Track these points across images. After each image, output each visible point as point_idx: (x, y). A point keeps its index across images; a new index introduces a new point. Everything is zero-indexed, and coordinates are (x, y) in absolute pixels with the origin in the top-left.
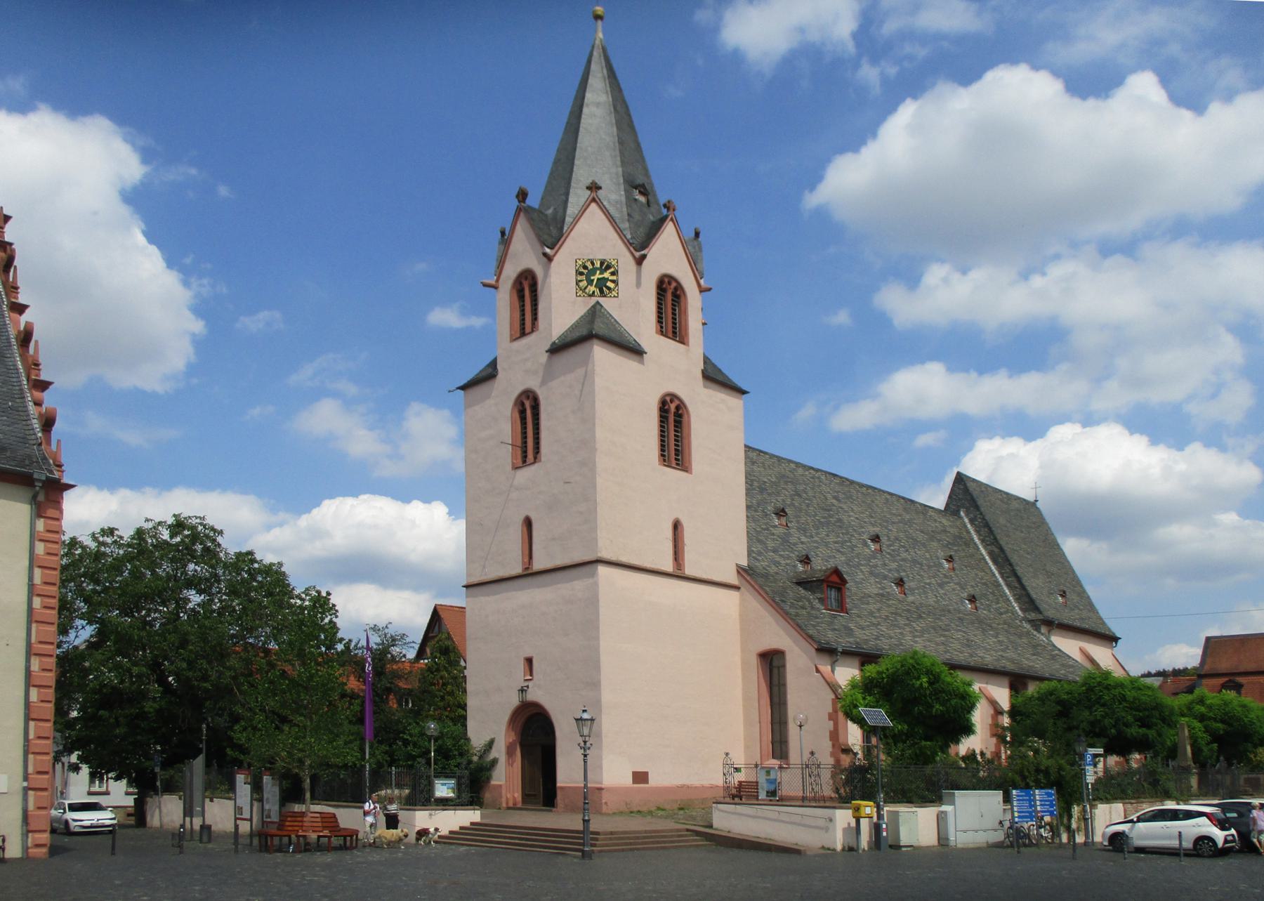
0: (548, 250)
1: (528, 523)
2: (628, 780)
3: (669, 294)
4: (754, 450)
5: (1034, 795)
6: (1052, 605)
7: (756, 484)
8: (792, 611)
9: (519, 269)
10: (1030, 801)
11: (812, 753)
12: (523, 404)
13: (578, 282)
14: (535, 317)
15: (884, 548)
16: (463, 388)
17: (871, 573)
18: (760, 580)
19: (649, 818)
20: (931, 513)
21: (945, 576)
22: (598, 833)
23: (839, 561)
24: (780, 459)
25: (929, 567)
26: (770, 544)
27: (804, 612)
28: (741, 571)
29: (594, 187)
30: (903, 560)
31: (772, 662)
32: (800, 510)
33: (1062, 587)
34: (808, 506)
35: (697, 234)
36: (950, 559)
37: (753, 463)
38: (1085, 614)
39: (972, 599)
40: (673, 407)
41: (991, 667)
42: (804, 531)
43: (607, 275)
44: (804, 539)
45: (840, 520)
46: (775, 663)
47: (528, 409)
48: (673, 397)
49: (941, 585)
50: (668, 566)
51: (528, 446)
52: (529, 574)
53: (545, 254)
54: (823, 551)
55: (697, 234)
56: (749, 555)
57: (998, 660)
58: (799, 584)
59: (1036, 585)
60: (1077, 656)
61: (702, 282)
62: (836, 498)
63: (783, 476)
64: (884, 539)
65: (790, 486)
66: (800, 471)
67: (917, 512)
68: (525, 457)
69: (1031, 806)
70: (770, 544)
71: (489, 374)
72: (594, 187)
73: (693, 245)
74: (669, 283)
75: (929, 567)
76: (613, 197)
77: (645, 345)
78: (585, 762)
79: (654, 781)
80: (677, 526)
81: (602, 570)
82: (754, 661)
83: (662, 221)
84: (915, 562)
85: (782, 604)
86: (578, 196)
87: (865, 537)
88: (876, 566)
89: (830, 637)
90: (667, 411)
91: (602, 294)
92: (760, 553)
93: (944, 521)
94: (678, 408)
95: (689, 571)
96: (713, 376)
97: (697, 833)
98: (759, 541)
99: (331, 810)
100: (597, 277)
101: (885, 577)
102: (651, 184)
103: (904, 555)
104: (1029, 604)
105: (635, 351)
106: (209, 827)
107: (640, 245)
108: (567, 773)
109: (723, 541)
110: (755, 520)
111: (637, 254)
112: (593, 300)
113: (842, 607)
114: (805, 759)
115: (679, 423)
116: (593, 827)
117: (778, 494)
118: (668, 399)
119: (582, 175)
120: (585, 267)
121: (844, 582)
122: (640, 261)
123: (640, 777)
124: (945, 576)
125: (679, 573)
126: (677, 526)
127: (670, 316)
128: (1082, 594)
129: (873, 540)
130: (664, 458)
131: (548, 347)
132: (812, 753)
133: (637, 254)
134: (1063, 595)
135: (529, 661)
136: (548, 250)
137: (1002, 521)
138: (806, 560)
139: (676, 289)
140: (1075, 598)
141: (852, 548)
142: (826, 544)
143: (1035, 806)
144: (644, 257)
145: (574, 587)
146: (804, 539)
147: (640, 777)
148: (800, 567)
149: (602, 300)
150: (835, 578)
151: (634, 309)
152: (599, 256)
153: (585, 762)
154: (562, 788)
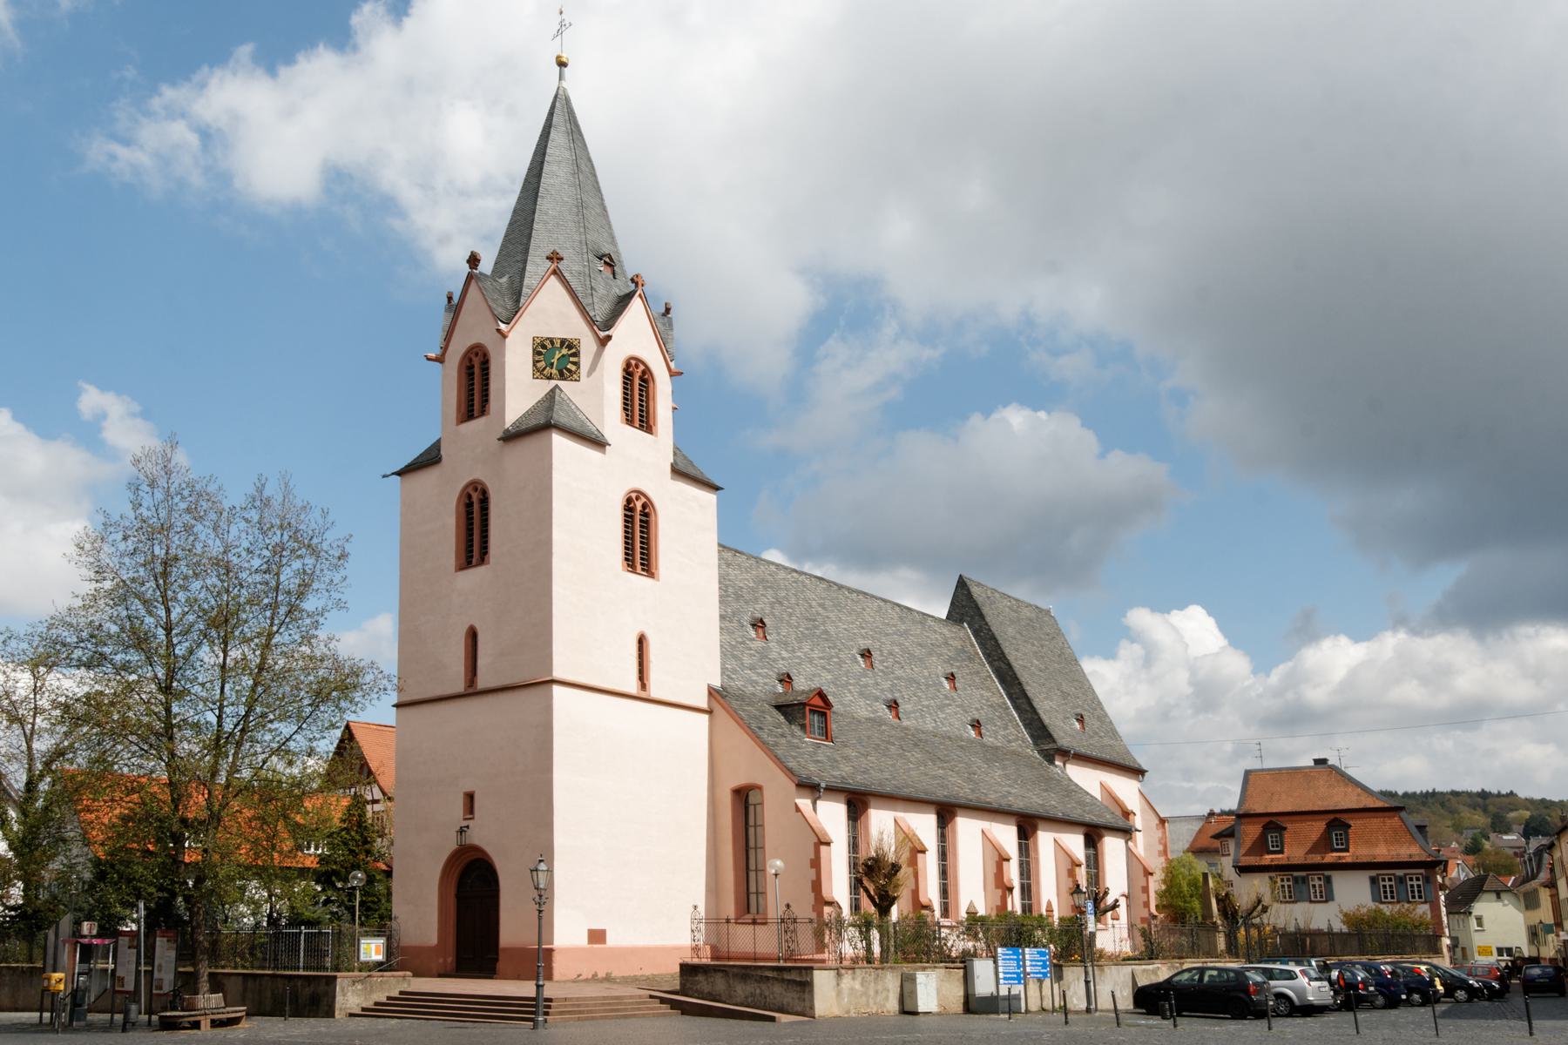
0: (503, 326)
1: (472, 635)
2: (582, 940)
3: (636, 380)
4: (730, 549)
5: (1023, 954)
6: (1065, 731)
8: (770, 740)
9: (469, 343)
10: (1018, 960)
11: (788, 906)
12: (470, 497)
13: (535, 363)
15: (876, 664)
16: (399, 473)
17: (861, 694)
18: (735, 704)
19: (607, 985)
20: (930, 622)
21: (946, 697)
22: (550, 1000)
23: (824, 681)
25: (928, 686)
26: (747, 660)
27: (783, 741)
28: (712, 692)
30: (898, 678)
31: (744, 798)
32: (781, 620)
33: (1079, 711)
34: (790, 615)
35: (668, 310)
36: (951, 678)
37: (728, 565)
38: (1107, 741)
39: (976, 725)
40: (639, 505)
41: (995, 805)
42: (784, 644)
43: (565, 351)
45: (826, 632)
46: (752, 800)
47: (475, 512)
48: (640, 494)
49: (941, 708)
50: (632, 686)
51: (474, 542)
52: (472, 690)
53: (499, 331)
54: (809, 669)
55: (668, 310)
56: (723, 673)
57: (1004, 797)
58: (778, 707)
59: (1047, 707)
60: (1096, 793)
61: (672, 365)
62: (822, 606)
63: (763, 581)
64: (875, 654)
65: (770, 592)
66: (782, 574)
67: (914, 622)
70: (747, 660)
71: (430, 459)
72: (554, 257)
73: (663, 318)
75: (928, 686)
76: (576, 268)
77: (608, 435)
78: (540, 918)
79: (612, 940)
80: (641, 641)
81: (556, 688)
82: (726, 800)
83: (628, 297)
84: (911, 681)
85: (760, 733)
86: (537, 265)
87: (854, 651)
88: (866, 686)
89: (812, 771)
90: (632, 510)
91: (562, 377)
92: (734, 671)
93: (945, 631)
94: (644, 506)
95: (654, 692)
96: (680, 472)
97: (663, 1001)
98: (734, 657)
99: (1387, 909)
100: (556, 359)
101: (877, 699)
102: (617, 252)
103: (899, 672)
104: (1039, 731)
105: (598, 443)
107: (603, 327)
108: (512, 930)
109: (693, 660)
110: (730, 633)
111: (602, 334)
112: (553, 383)
113: (826, 734)
114: (780, 913)
115: (646, 525)
116: (547, 993)
117: (756, 600)
119: (541, 244)
120: (544, 347)
121: (828, 704)
122: (604, 342)
123: (597, 936)
124: (946, 697)
125: (643, 695)
126: (641, 641)
127: (638, 412)
128: (1103, 717)
129: (862, 656)
131: (500, 434)
132: (788, 906)
133: (602, 334)
134: (1081, 719)
135: (470, 798)
136: (503, 326)
137: (1011, 631)
138: (786, 679)
139: (644, 372)
141: (840, 663)
142: (811, 661)
143: (1024, 966)
144: (609, 338)
145: (406, 698)
147: (597, 936)
148: (780, 689)
149: (561, 384)
150: (818, 701)
151: (598, 395)
152: (559, 333)
153: (540, 918)
154: (505, 949)
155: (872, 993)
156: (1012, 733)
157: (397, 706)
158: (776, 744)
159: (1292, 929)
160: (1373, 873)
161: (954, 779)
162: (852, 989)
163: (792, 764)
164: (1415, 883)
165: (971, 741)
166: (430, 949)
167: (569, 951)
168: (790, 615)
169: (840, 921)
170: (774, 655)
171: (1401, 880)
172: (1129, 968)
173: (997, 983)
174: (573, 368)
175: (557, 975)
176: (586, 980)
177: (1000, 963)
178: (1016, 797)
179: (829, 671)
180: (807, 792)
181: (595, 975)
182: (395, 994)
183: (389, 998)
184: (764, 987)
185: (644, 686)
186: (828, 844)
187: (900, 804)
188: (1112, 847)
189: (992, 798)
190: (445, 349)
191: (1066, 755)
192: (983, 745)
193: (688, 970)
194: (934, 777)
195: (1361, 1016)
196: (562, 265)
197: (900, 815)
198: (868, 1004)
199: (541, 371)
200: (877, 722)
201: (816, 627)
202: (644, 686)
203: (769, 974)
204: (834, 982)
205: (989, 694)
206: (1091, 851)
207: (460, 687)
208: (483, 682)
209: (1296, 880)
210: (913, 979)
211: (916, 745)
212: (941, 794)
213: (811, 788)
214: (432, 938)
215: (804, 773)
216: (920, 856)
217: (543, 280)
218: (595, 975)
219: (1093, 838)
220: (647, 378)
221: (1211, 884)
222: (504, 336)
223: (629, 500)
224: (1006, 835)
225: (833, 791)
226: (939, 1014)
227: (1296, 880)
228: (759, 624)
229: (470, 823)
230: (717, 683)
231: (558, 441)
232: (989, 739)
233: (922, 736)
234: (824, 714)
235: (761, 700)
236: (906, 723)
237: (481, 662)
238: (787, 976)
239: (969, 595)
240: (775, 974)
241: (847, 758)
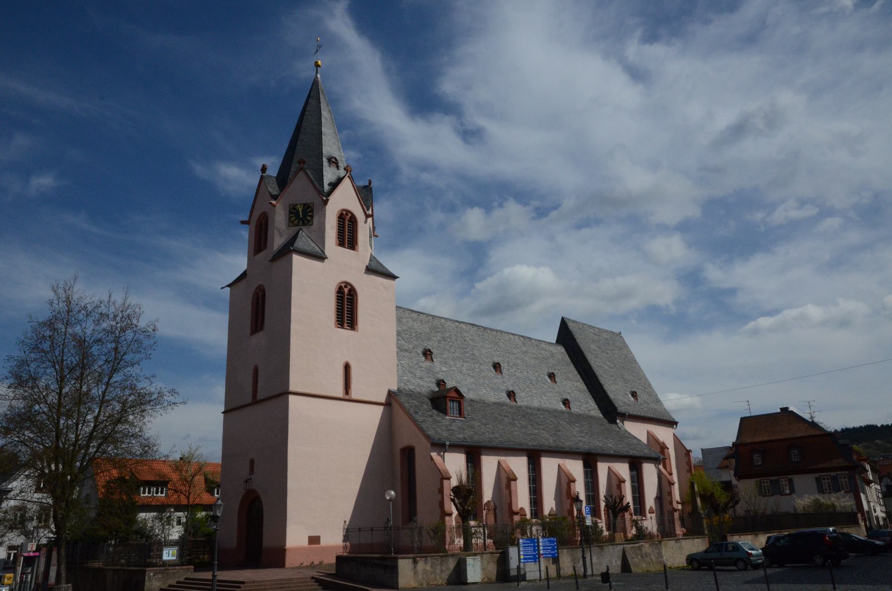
2: (305, 543)
10: (534, 547)
13: (290, 218)
24: (434, 317)
26: (418, 373)
29: (302, 162)
30: (518, 378)
38: (652, 405)
40: (346, 290)
42: (444, 363)
44: (444, 369)
45: (473, 354)
48: (347, 284)
50: (340, 393)
52: (255, 401)
60: (644, 439)
62: (473, 341)
74: (347, 214)
79: (324, 542)
80: (347, 367)
81: (291, 397)
90: (343, 293)
94: (350, 291)
106: (535, 561)
118: (343, 285)
125: (347, 397)
126: (347, 367)
130: (340, 323)
135: (252, 462)
136: (274, 202)
140: (646, 397)
143: (539, 550)
146: (444, 369)
154: (290, 549)
155: (438, 572)
156: (586, 405)
158: (424, 421)
159: (769, 512)
160: (818, 475)
162: (425, 570)
163: (431, 432)
165: (562, 412)
170: (437, 369)
172: (622, 547)
173: (520, 562)
174: (309, 218)
175: (287, 564)
177: (521, 549)
179: (472, 377)
181: (313, 563)
182: (182, 579)
183: (178, 582)
189: (567, 444)
190: (250, 216)
191: (625, 417)
192: (570, 414)
195: (721, 576)
196: (305, 166)
197: (502, 458)
198: (435, 579)
199: (293, 222)
200: (499, 405)
201: (466, 353)
203: (376, 562)
204: (412, 566)
206: (635, 473)
207: (249, 400)
208: (260, 396)
209: (771, 481)
210: (465, 561)
211: (524, 416)
212: (531, 444)
215: (437, 437)
217: (296, 173)
218: (313, 563)
219: (636, 465)
220: (353, 220)
224: (576, 468)
225: (455, 447)
226: (480, 583)
227: (771, 481)
228: (427, 354)
229: (252, 477)
230: (394, 388)
231: (296, 259)
233: (530, 411)
235: (424, 396)
236: (519, 403)
237: (259, 385)
241: (472, 427)
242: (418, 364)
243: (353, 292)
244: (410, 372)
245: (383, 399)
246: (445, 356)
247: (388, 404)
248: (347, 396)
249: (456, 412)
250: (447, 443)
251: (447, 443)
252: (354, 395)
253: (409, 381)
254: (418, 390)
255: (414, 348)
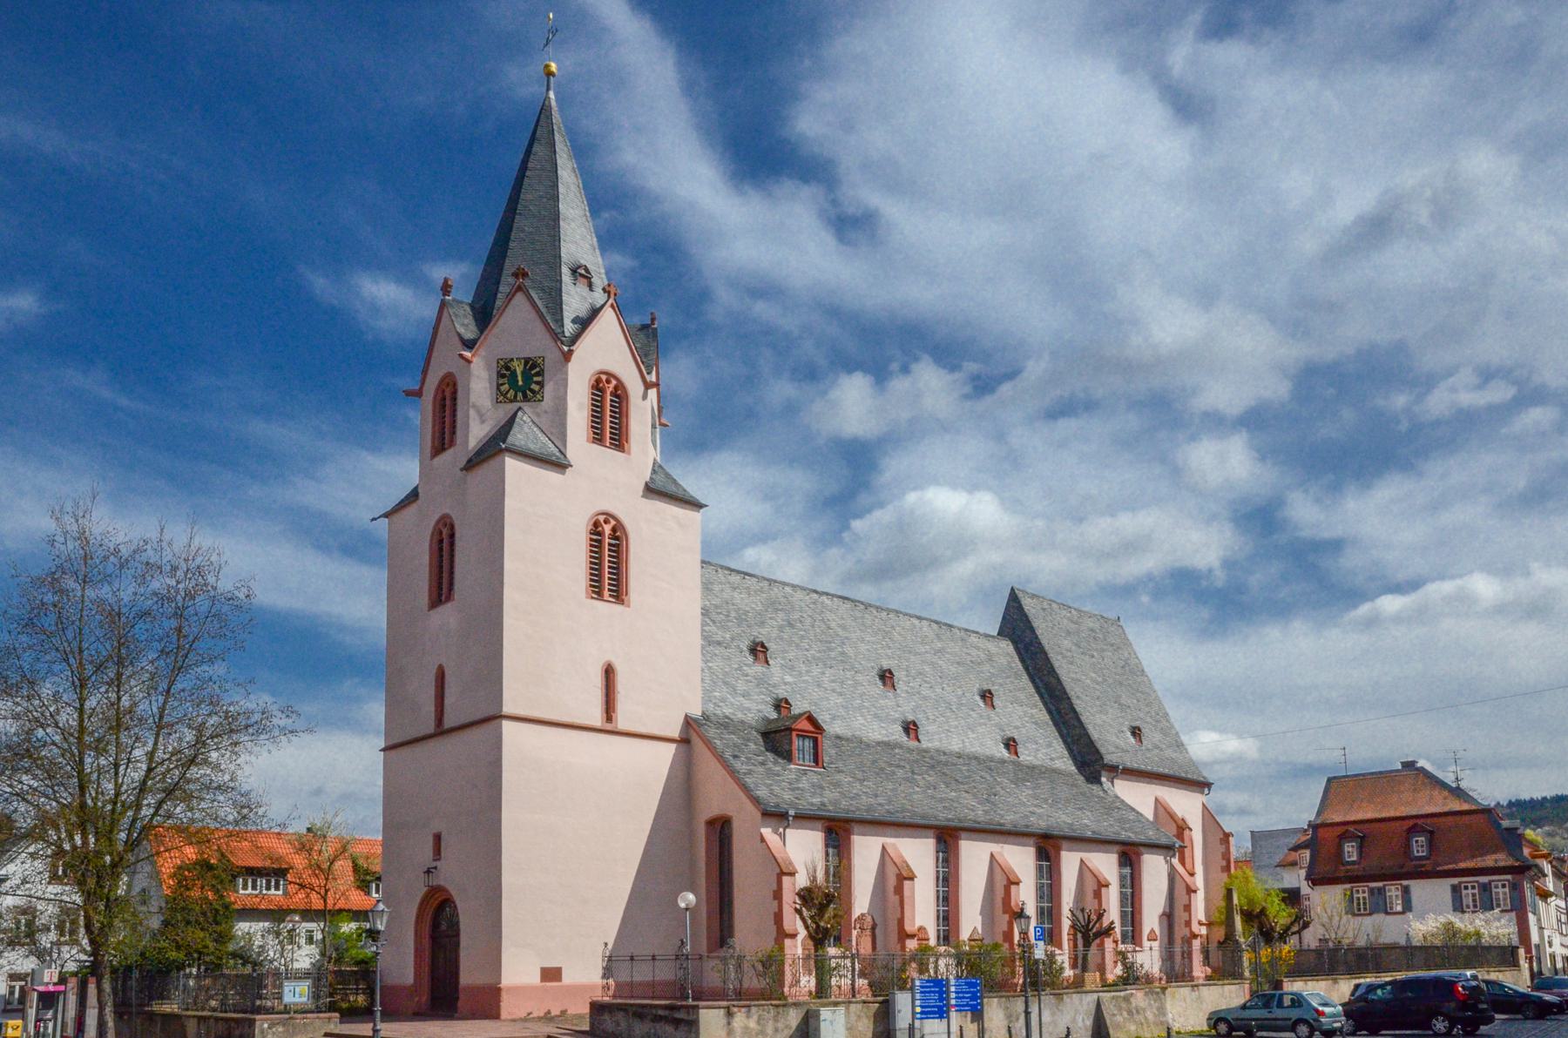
2: (535, 979)
7: (733, 614)
9: (441, 374)
13: (499, 386)
14: (453, 433)
16: (386, 515)
17: (876, 716)
27: (761, 769)
30: (925, 698)
38: (1169, 753)
40: (607, 529)
41: (1009, 827)
42: (789, 668)
44: (788, 679)
45: (843, 653)
48: (609, 516)
50: (597, 719)
52: (441, 731)
62: (844, 627)
66: (799, 595)
68: (440, 595)
69: (941, 999)
74: (608, 382)
79: (567, 978)
80: (609, 672)
81: (506, 724)
94: (614, 530)
95: (622, 723)
118: (602, 518)
125: (609, 727)
126: (609, 672)
130: (596, 590)
135: (438, 838)
136: (468, 354)
139: (616, 388)
143: (948, 999)
145: (391, 742)
155: (770, 1030)
157: (383, 750)
158: (750, 772)
159: (1361, 942)
161: (969, 800)
162: (746, 1027)
163: (762, 793)
164: (1500, 890)
165: (1003, 762)
166: (405, 988)
167: (517, 990)
168: (802, 637)
169: (924, 950)
171: (1485, 888)
174: (535, 387)
176: (540, 1019)
178: (1040, 816)
180: (773, 821)
184: (658, 1026)
185: (609, 719)
186: (792, 874)
187: (890, 830)
188: (1154, 869)
189: (1009, 819)
191: (1115, 771)
192: (1017, 765)
193: (597, 1009)
194: (942, 800)
197: (889, 841)
201: (830, 649)
202: (609, 719)
203: (661, 1012)
204: (724, 1021)
205: (1023, 713)
206: (1127, 871)
207: (430, 727)
208: (449, 722)
211: (933, 767)
212: (943, 816)
213: (777, 816)
214: (409, 979)
216: (906, 883)
217: (510, 298)
220: (620, 394)
221: (1236, 901)
222: (469, 362)
223: (596, 524)
224: (1021, 860)
225: (805, 818)
227: (1372, 891)
229: (438, 864)
230: (696, 711)
232: (1026, 756)
233: (943, 758)
234: (815, 741)
236: (925, 744)
238: (678, 1015)
239: (1020, 608)
240: (667, 1013)
241: (837, 785)
242: (739, 668)
243: (619, 533)
244: (725, 683)
245: (675, 731)
246: (791, 655)
247: (684, 741)
248: (609, 723)
249: (809, 757)
250: (792, 812)
251: (792, 812)
252: (622, 723)
253: (723, 700)
254: (740, 715)
255: (733, 639)
